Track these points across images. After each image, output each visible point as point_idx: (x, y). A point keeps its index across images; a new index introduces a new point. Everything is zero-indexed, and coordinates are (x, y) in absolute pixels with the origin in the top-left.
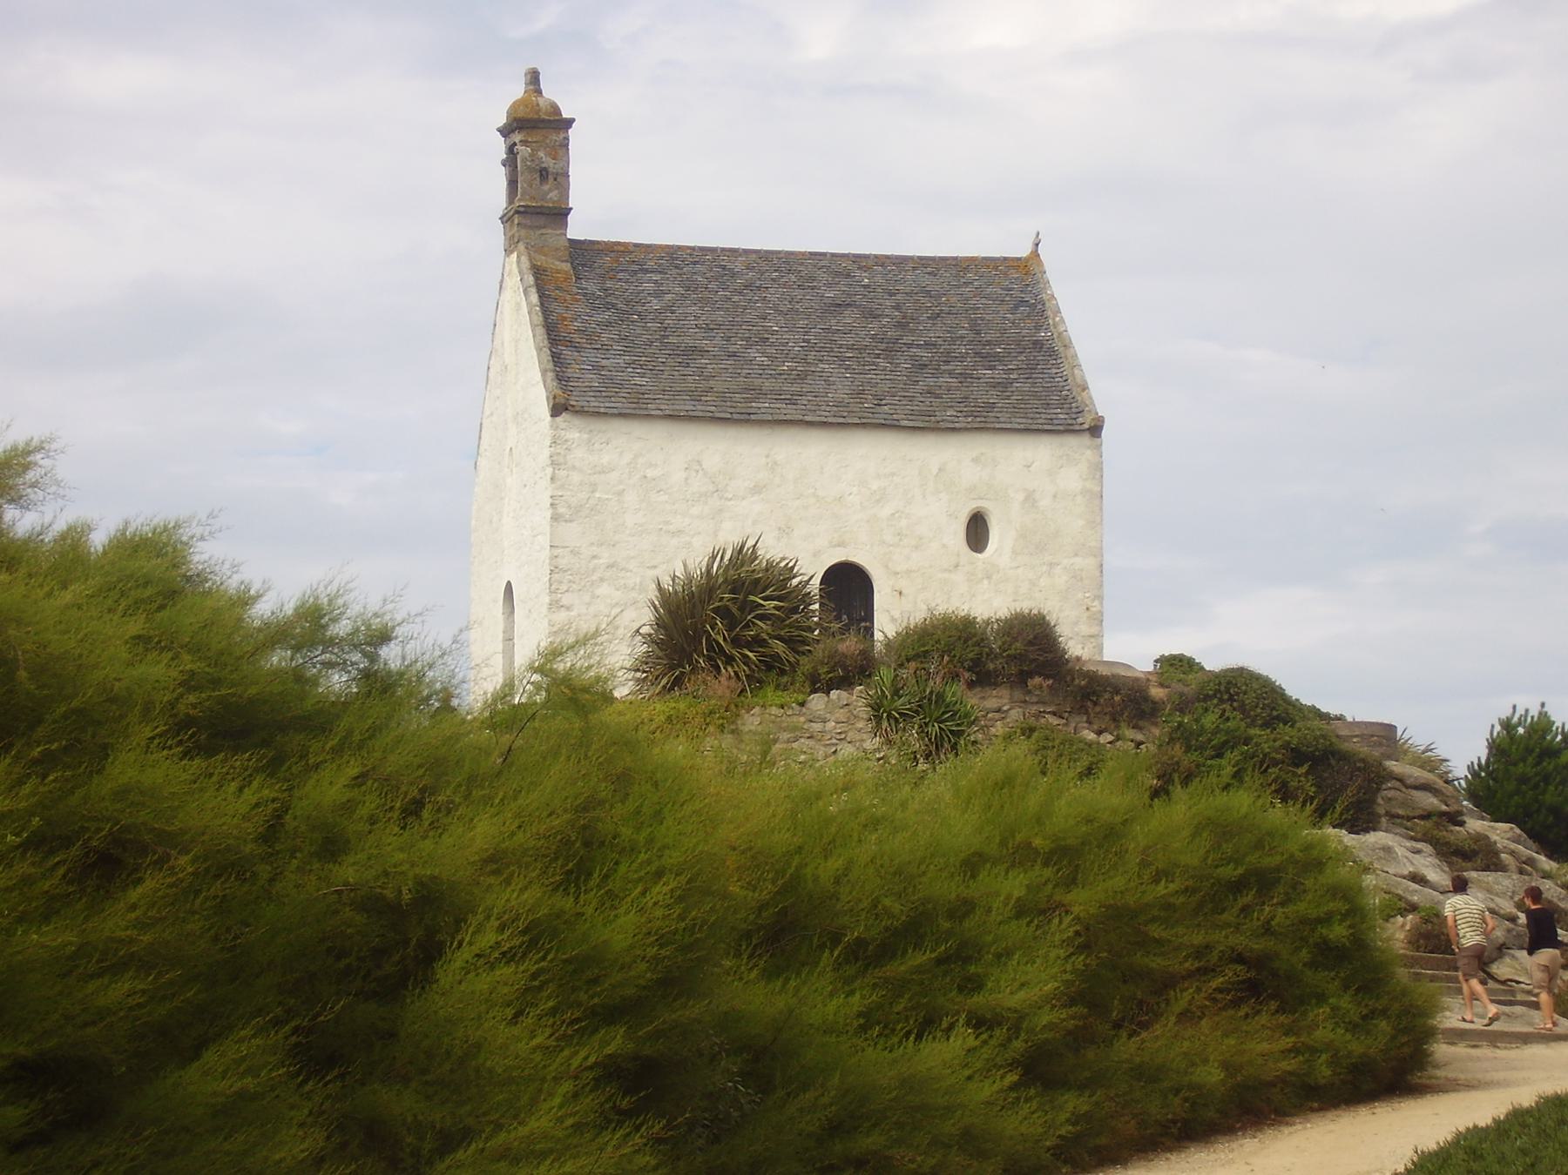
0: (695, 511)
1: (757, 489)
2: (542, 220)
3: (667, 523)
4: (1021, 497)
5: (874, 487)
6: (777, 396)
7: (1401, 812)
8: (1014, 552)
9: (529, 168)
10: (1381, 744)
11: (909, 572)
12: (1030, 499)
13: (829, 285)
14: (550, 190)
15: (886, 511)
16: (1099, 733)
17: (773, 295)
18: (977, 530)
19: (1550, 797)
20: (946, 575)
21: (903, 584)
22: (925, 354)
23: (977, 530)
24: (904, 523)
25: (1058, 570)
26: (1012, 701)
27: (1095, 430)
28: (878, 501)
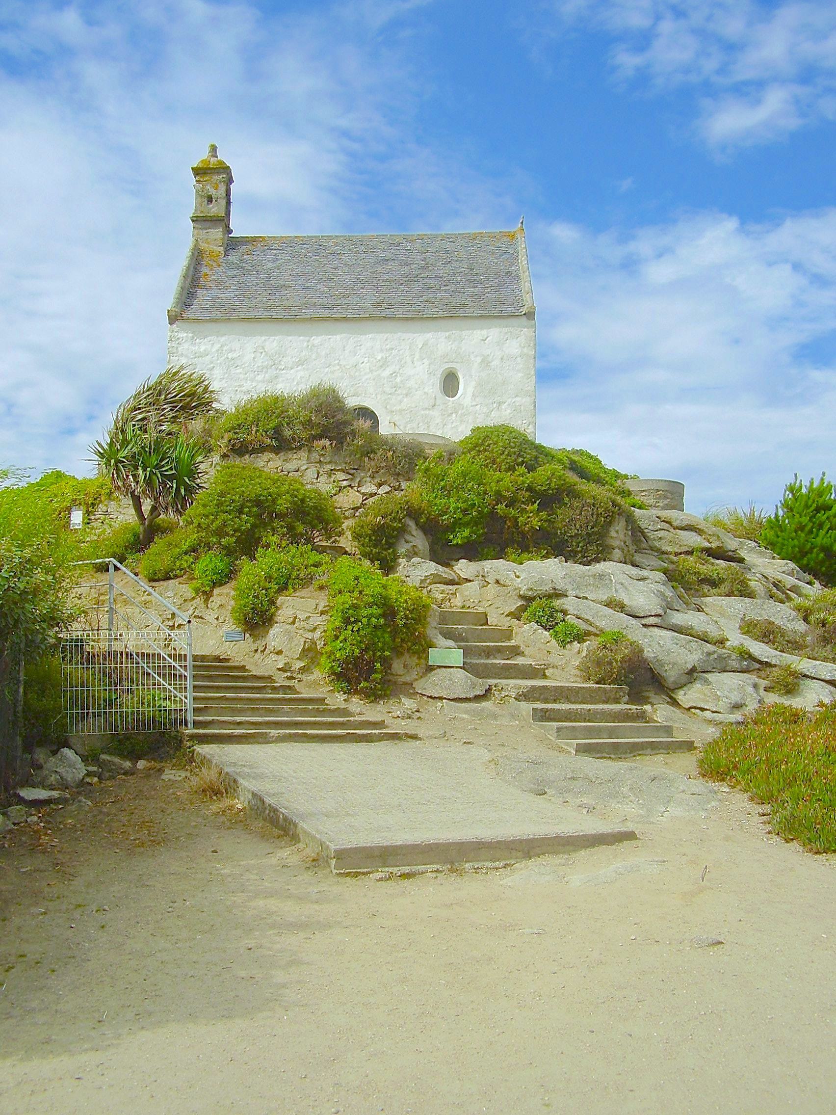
0: (260, 378)
1: (300, 363)
2: (208, 224)
3: (240, 386)
4: (479, 359)
5: (379, 358)
6: (325, 308)
7: (669, 549)
8: (474, 396)
9: (201, 196)
10: (666, 497)
11: (401, 411)
12: (486, 362)
13: (384, 250)
14: (213, 207)
15: (387, 373)
16: (380, 485)
17: (346, 258)
18: (450, 383)
19: (822, 538)
20: (427, 412)
21: (396, 418)
22: (432, 282)
23: (450, 383)
24: (398, 380)
25: (503, 407)
26: (309, 461)
27: (530, 315)
28: (381, 366)
